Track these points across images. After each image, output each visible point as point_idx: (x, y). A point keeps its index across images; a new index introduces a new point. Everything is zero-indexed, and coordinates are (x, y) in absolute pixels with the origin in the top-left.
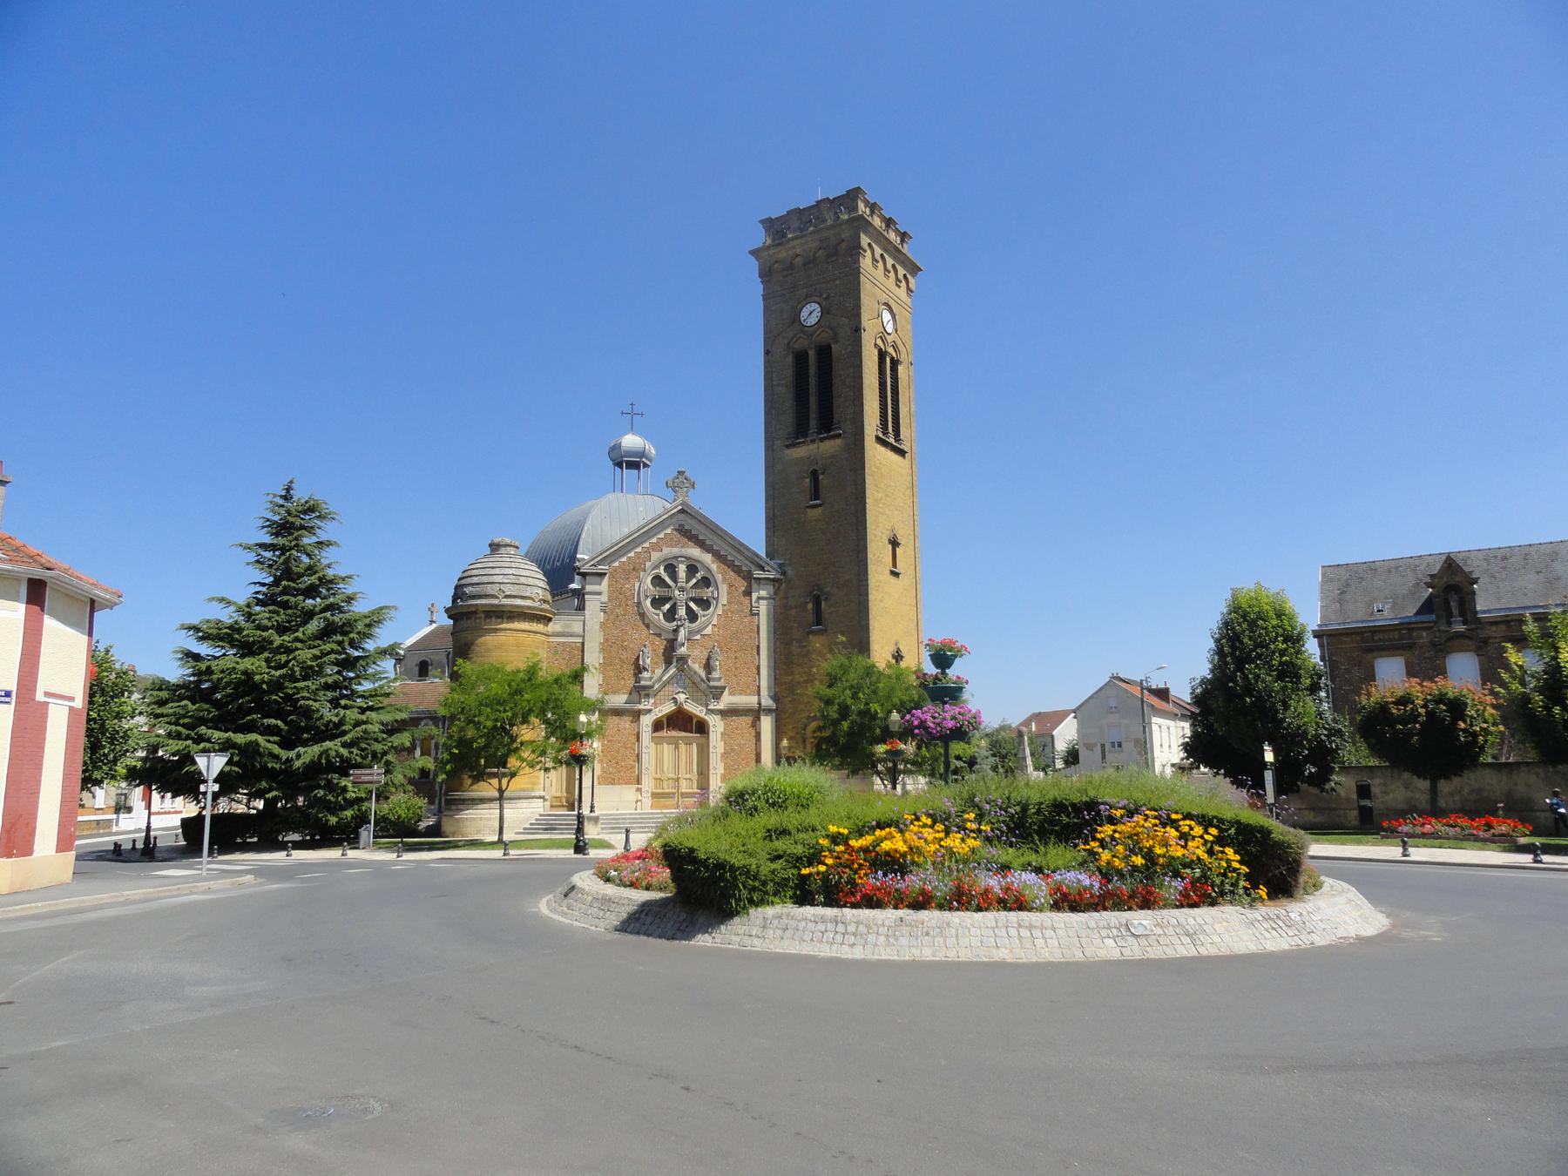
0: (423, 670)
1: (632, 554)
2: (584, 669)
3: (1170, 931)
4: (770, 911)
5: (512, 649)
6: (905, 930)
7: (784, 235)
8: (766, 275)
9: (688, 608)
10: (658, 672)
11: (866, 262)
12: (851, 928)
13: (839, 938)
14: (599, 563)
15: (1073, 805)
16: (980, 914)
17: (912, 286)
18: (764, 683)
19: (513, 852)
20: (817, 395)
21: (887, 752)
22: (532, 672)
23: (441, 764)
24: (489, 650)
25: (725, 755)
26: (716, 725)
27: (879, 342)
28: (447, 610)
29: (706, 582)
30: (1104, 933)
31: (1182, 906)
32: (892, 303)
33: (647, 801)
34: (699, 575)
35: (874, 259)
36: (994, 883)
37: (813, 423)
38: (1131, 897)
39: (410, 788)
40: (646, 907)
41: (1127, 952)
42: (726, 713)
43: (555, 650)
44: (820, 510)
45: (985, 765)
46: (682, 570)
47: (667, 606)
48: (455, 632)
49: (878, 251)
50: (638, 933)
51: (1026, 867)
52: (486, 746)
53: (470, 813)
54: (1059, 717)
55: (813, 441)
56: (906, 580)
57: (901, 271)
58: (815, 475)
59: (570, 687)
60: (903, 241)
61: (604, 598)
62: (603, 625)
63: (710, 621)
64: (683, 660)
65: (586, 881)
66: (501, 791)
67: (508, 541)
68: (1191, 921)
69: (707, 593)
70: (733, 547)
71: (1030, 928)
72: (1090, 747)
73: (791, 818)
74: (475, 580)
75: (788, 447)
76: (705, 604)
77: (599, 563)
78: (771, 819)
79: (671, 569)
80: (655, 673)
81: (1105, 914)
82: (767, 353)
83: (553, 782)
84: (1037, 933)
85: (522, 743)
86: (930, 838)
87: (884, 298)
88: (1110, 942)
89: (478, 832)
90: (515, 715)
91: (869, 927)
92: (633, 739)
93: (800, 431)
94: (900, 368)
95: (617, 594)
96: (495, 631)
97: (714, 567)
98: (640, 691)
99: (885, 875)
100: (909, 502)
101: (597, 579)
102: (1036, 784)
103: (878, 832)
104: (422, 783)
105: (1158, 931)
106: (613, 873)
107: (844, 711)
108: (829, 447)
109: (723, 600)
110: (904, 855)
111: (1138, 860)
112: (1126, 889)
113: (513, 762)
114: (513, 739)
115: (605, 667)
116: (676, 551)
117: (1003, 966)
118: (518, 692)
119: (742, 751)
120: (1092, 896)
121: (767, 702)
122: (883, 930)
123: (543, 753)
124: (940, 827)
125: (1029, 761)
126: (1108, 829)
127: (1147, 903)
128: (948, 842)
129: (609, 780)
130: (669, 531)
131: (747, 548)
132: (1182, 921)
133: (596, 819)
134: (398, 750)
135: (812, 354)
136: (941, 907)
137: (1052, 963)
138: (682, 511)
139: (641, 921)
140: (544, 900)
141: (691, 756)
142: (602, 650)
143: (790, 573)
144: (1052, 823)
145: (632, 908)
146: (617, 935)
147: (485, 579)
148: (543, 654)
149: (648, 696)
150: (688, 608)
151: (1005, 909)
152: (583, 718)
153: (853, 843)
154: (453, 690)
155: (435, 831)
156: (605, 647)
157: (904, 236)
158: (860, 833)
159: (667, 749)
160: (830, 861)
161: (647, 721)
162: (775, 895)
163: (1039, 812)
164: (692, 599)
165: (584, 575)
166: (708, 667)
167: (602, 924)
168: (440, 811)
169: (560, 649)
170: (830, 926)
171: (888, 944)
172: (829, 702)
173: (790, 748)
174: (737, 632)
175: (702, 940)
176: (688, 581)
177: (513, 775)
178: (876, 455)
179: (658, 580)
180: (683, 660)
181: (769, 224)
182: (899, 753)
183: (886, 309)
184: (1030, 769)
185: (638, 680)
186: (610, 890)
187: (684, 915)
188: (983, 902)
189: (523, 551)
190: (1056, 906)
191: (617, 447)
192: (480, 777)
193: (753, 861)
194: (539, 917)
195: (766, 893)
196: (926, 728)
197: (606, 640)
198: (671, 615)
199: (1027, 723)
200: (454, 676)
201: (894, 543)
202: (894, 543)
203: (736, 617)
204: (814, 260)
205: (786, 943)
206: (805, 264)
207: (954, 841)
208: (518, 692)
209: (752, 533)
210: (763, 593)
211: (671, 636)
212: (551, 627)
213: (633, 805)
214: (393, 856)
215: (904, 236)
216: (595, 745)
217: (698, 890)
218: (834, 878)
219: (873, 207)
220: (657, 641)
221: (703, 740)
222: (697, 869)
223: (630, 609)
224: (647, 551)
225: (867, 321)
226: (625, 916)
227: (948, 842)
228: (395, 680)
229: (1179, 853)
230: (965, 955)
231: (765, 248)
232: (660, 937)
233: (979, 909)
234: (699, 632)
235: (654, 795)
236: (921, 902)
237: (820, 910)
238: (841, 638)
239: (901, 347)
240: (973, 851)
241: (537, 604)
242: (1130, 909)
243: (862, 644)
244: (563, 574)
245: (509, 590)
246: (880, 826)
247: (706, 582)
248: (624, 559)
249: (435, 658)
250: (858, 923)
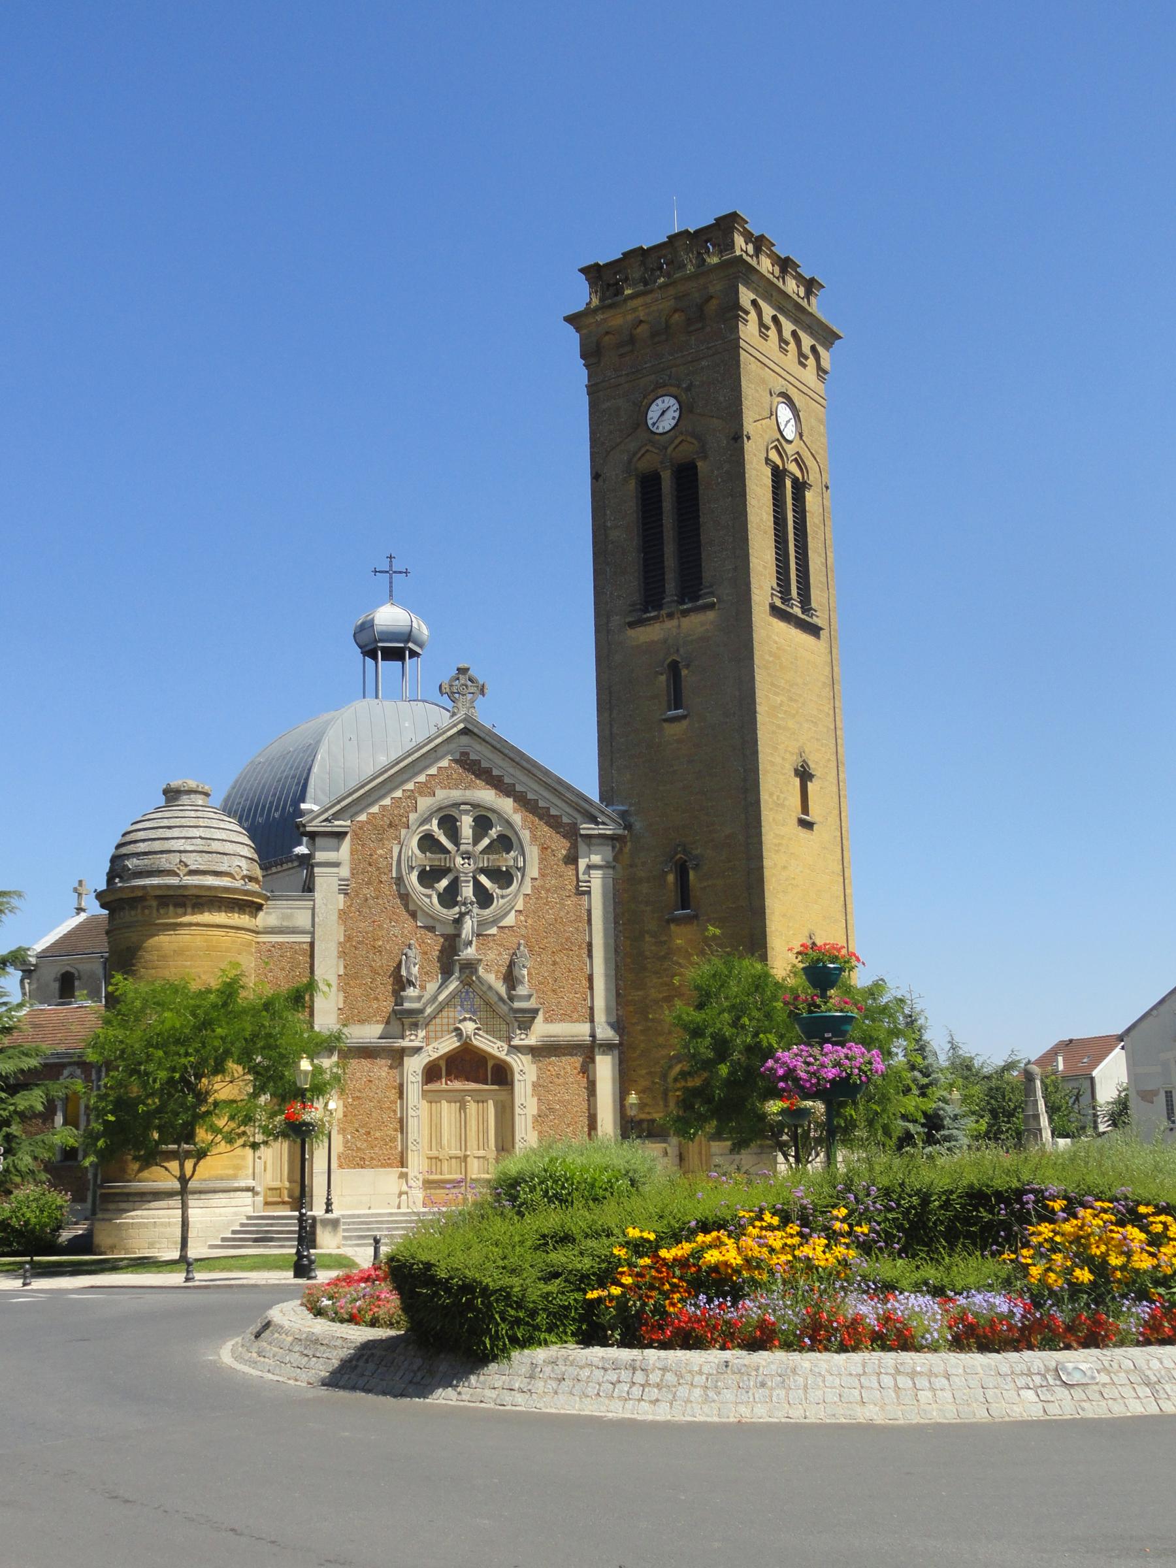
0: (67, 986)
1: (387, 801)
2: (311, 986)
3: (1121, 1378)
4: (540, 1354)
5: (202, 954)
6: (731, 1379)
7: (619, 292)
8: (591, 354)
9: (478, 886)
10: (432, 987)
11: (749, 330)
12: (655, 1377)
13: (636, 1391)
14: (336, 816)
15: (998, 1194)
16: (844, 1356)
17: (826, 364)
18: (600, 1003)
19: (200, 1276)
20: (674, 538)
21: (783, 1112)
22: (230, 990)
23: (92, 1137)
24: (164, 958)
25: (540, 1118)
26: (525, 1071)
27: (774, 456)
28: (99, 896)
29: (505, 843)
30: (1021, 1382)
31: (1148, 1342)
32: (793, 393)
33: (418, 1195)
34: (493, 833)
35: (762, 325)
36: (867, 1310)
37: (671, 586)
38: (1070, 1329)
39: (44, 1176)
40: (368, 1347)
41: (1054, 1411)
42: (544, 1051)
43: (268, 954)
44: (685, 723)
45: (964, 1130)
46: (466, 824)
47: (444, 883)
48: (113, 928)
49: (768, 311)
50: (354, 1388)
51: (917, 1288)
52: (159, 1110)
53: (138, 1216)
54: (1099, 1048)
55: (670, 616)
56: (824, 833)
57: (807, 341)
58: (674, 669)
59: (288, 1015)
60: (809, 293)
61: (345, 871)
62: (343, 915)
63: (512, 903)
64: (470, 967)
65: (290, 1316)
66: (183, 1180)
67: (192, 784)
68: (1155, 1364)
69: (507, 860)
70: (548, 787)
71: (913, 1374)
72: (1147, 1096)
73: (578, 1218)
74: (142, 847)
75: (631, 625)
76: (504, 878)
77: (336, 816)
78: (551, 1219)
79: (449, 824)
80: (429, 989)
81: (1027, 1354)
82: (596, 476)
83: (269, 1164)
84: (922, 1382)
85: (216, 1104)
86: (777, 1245)
87: (779, 385)
88: (1030, 1395)
89: (151, 1246)
90: (203, 1061)
91: (680, 1376)
92: (393, 1094)
93: (651, 600)
94: (809, 495)
95: (364, 864)
96: (175, 926)
97: (517, 819)
98: (403, 1018)
99: (710, 1301)
100: (828, 708)
101: (332, 842)
102: (961, 1162)
103: (700, 1238)
104: (63, 1169)
105: (1103, 1378)
106: (326, 1302)
107: (722, 1048)
108: (697, 624)
109: (533, 871)
110: (737, 1272)
111: (1084, 1276)
112: (1061, 1317)
113: (202, 1135)
114: (201, 1097)
115: (347, 980)
116: (456, 795)
117: (867, 1429)
118: (207, 1024)
119: (566, 1110)
120: (1011, 1328)
121: (605, 1032)
122: (700, 1380)
123: (248, 1120)
124: (794, 1228)
125: (1044, 1121)
126: (1045, 1229)
127: (1092, 1340)
128: (806, 1251)
129: (356, 1160)
130: (444, 763)
131: (569, 788)
132: (1141, 1363)
133: (335, 1223)
134: (24, 1117)
135: (667, 478)
136: (788, 1346)
137: (939, 1426)
138: (465, 732)
139: (359, 1372)
140: (229, 1345)
141: (485, 1121)
142: (343, 954)
143: (638, 826)
144: (967, 1221)
145: (345, 1353)
146: (323, 1392)
147: (157, 846)
148: (249, 963)
149: (415, 1026)
150: (478, 886)
151: (884, 1348)
152: (305, 1065)
153: (663, 1253)
154: (108, 1022)
155: (84, 1244)
156: (346, 951)
157: (811, 285)
158: (676, 1238)
159: (447, 1110)
160: (627, 1280)
161: (414, 1066)
162: (549, 1330)
163: (946, 1205)
164: (483, 871)
165: (313, 836)
166: (511, 979)
167: (300, 1376)
168: (94, 1213)
169: (276, 953)
170: (625, 1375)
171: (706, 1400)
172: (697, 1032)
173: (642, 1106)
174: (555, 921)
175: (444, 1397)
176: (476, 841)
177: (201, 1154)
178: (773, 637)
179: (428, 842)
180: (470, 967)
181: (593, 273)
182: (804, 1113)
183: (781, 399)
184: (1047, 1134)
185: (399, 1000)
186: (320, 1326)
187: (418, 1362)
188: (851, 1338)
189: (218, 799)
190: (958, 1344)
191: (366, 627)
192: (152, 1157)
193: (515, 1281)
194: (218, 1369)
195: (537, 1328)
196: (796, 1080)
197: (349, 938)
198: (450, 897)
199: (1048, 1058)
200: (112, 1001)
201: (804, 775)
202: (804, 775)
203: (553, 898)
204: (666, 321)
205: (562, 1398)
206: (654, 335)
207: (816, 1249)
208: (207, 1024)
209: (578, 765)
210: (596, 859)
211: (450, 930)
212: (263, 919)
213: (374, 1204)
214: (17, 1283)
215: (811, 285)
216: (332, 1105)
217: (440, 1323)
218: (634, 1304)
219: (759, 243)
220: (429, 938)
221: (503, 1096)
222: (436, 1294)
223: (385, 889)
224: (411, 796)
225: (750, 425)
226: (336, 1363)
227: (806, 1251)
228: (20, 1006)
229: (1144, 1263)
230: (815, 1414)
231: (588, 312)
232: (384, 1393)
233: (843, 1349)
234: (495, 922)
235: (428, 1184)
236: (760, 1339)
237: (614, 1353)
238: (713, 930)
239: (810, 462)
240: (844, 1263)
241: (238, 884)
242: (1068, 1347)
243: (752, 938)
244: (280, 832)
245: (195, 862)
246: (705, 1228)
247: (505, 843)
248: (375, 809)
249: (85, 967)
250: (664, 1370)
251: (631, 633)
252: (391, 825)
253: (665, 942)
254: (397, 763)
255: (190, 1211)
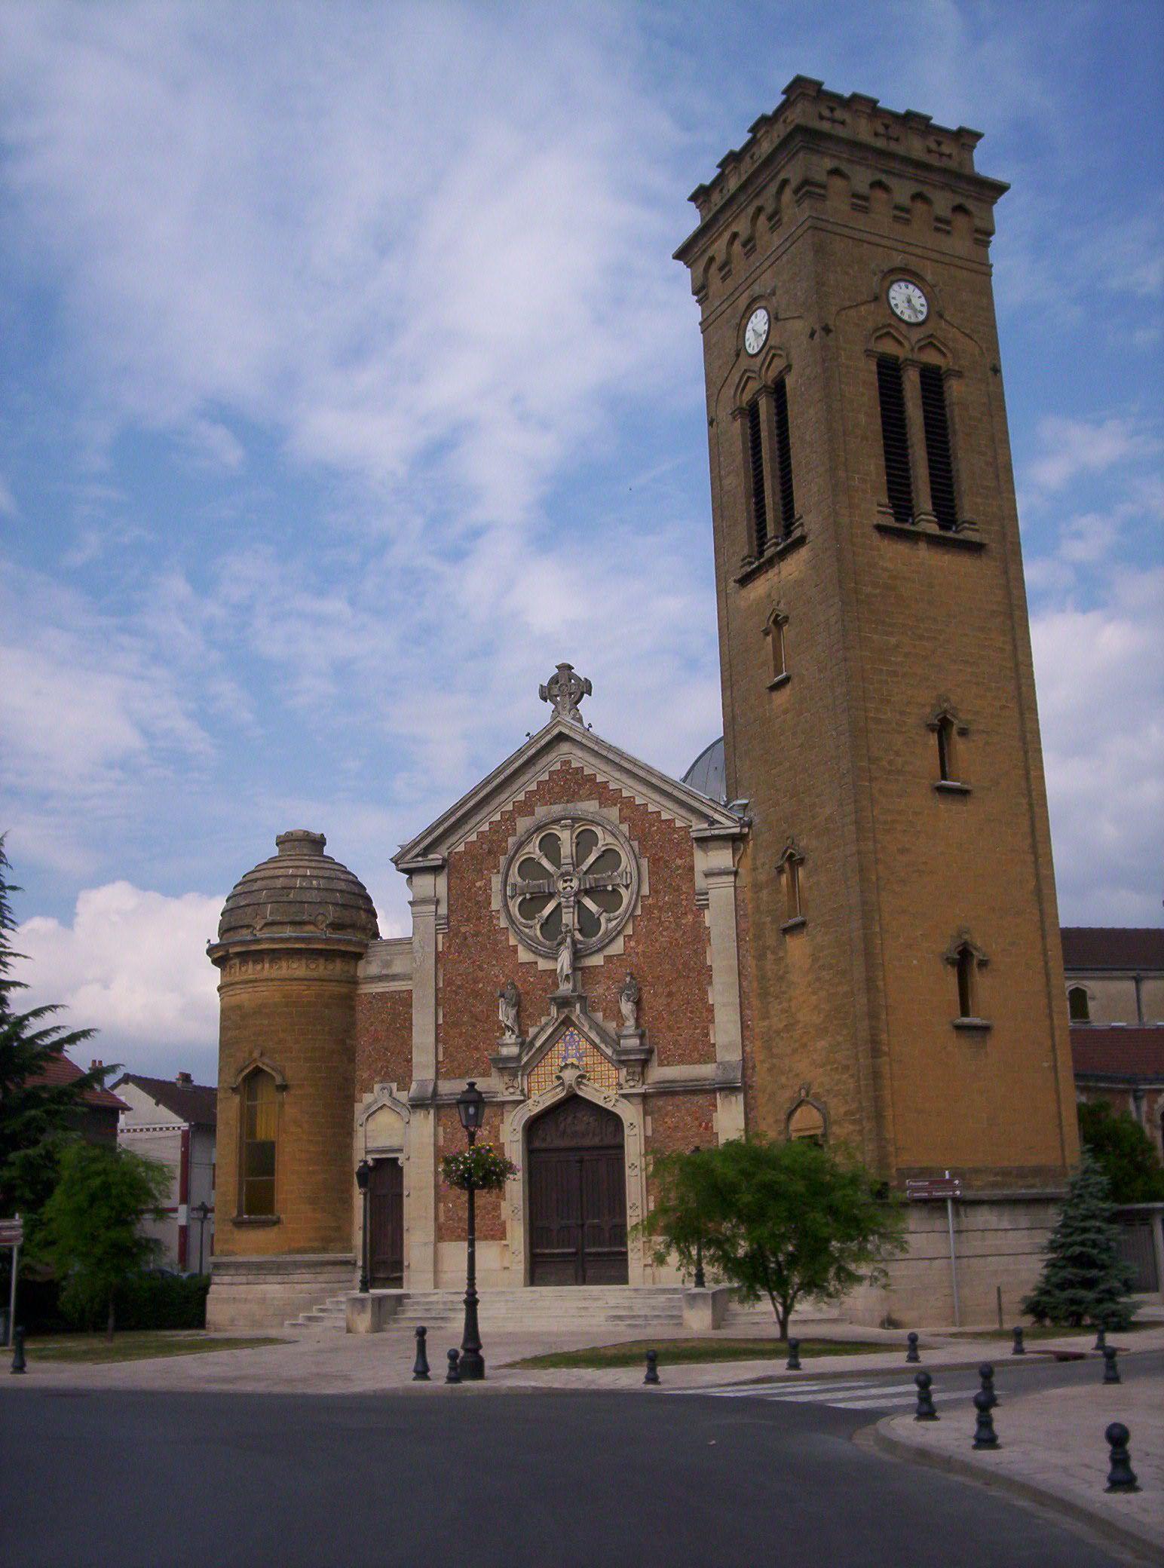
19: (808, 1364)
164: (588, 892)
197: (449, 982)
224: (510, 818)
251: (744, 592)
252: (490, 852)
253: (782, 958)
254: (476, 794)
255: (465, 1288)
